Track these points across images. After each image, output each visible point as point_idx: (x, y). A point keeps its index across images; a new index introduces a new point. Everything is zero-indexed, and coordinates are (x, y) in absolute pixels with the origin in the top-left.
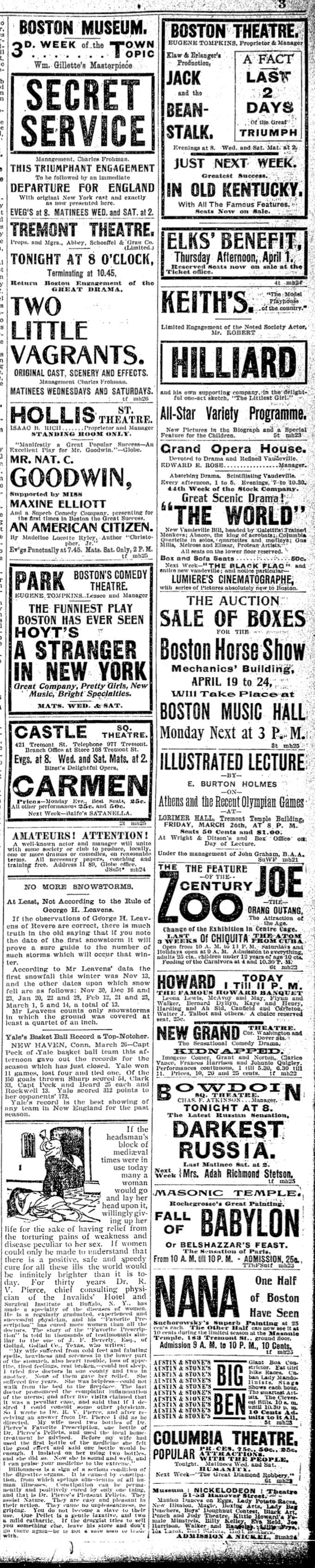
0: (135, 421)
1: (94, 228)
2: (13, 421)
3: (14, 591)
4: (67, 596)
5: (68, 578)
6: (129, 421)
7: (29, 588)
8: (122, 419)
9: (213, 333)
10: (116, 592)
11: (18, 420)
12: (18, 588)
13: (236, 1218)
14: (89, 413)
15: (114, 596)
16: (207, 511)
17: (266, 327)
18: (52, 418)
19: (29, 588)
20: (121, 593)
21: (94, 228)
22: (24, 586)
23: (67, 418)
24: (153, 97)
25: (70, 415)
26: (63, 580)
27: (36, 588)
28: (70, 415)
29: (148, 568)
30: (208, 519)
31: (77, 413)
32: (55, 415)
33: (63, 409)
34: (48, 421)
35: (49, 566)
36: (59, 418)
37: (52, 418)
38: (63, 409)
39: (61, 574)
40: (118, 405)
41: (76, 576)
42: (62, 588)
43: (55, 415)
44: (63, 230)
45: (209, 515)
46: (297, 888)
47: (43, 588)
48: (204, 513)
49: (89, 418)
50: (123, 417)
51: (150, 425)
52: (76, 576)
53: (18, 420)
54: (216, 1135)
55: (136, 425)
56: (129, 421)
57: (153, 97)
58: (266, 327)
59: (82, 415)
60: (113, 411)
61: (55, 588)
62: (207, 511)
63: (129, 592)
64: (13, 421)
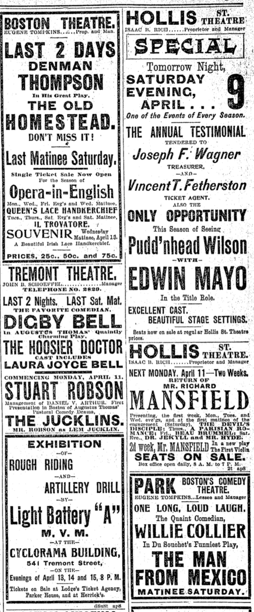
0: (233, 356)
1: (23, 81)
2: (132, 356)
3: (134, 495)
4: (179, 497)
5: (178, 483)
6: (228, 356)
7: (146, 492)
8: (222, 355)
9: (151, 320)
10: (219, 495)
11: (136, 355)
12: (136, 492)
13: (69, 345)
14: (194, 348)
15: (219, 498)
16: (180, 556)
17: (149, 333)
18: (165, 354)
19: (146, 492)
20: (224, 495)
21: (23, 81)
22: (141, 491)
23: (176, 354)
24: (177, 607)
25: (179, 351)
26: (174, 485)
27: (152, 492)
28: (179, 351)
29: (246, 477)
30: (180, 562)
31: (185, 349)
32: (167, 351)
33: (173, 347)
34: (162, 356)
35: (162, 475)
36: (167, 21)
37: (165, 354)
38: (173, 347)
39: (173, 480)
40: (219, 344)
41: (184, 482)
42: (174, 492)
43: (167, 351)
44: (182, 214)
45: (181, 559)
46: (140, 134)
47: (157, 492)
48: (177, 557)
49: (194, 354)
50: (222, 353)
51: (246, 359)
52: (184, 482)
53: (136, 355)
54: (173, 82)
55: (234, 359)
56: (228, 356)
57: (177, 607)
58: (149, 333)
59: (188, 352)
60: (215, 348)
61: (168, 492)
62: (180, 556)
63: (231, 494)
64: (132, 356)
